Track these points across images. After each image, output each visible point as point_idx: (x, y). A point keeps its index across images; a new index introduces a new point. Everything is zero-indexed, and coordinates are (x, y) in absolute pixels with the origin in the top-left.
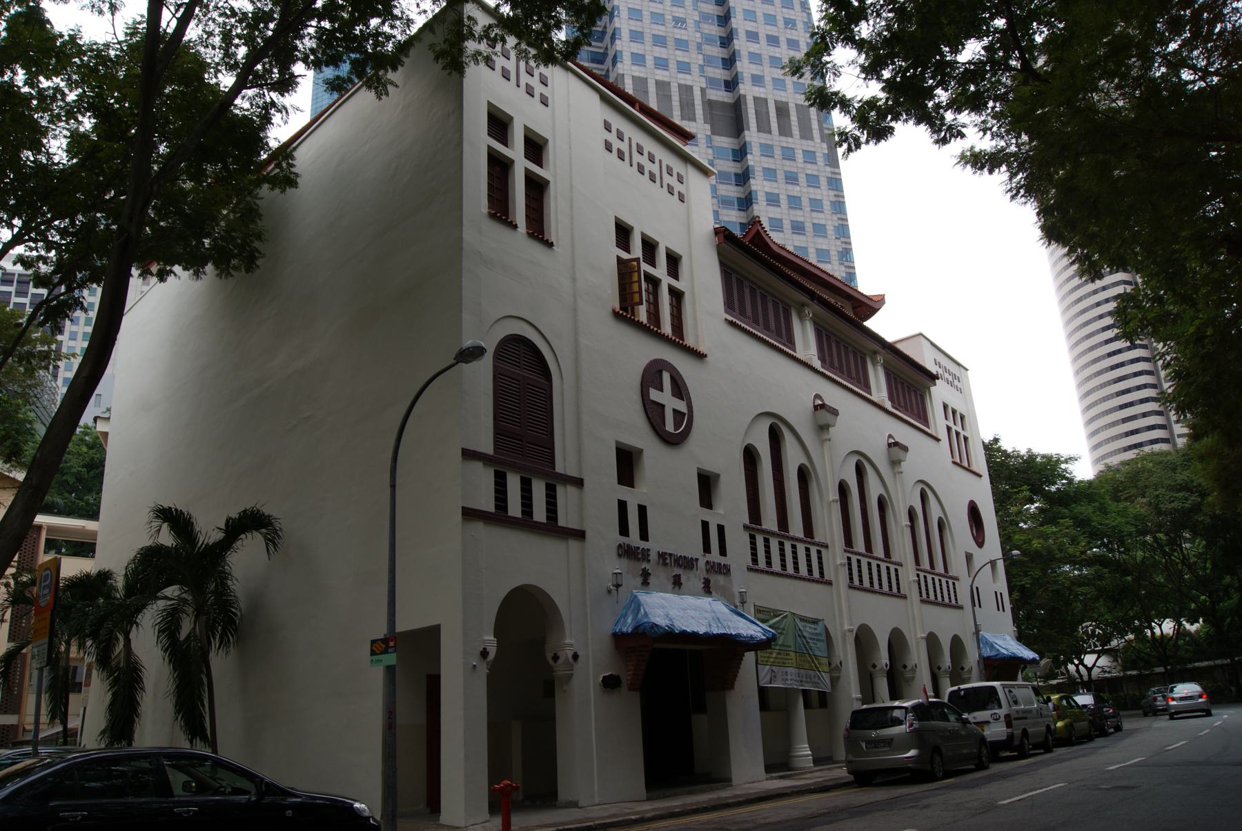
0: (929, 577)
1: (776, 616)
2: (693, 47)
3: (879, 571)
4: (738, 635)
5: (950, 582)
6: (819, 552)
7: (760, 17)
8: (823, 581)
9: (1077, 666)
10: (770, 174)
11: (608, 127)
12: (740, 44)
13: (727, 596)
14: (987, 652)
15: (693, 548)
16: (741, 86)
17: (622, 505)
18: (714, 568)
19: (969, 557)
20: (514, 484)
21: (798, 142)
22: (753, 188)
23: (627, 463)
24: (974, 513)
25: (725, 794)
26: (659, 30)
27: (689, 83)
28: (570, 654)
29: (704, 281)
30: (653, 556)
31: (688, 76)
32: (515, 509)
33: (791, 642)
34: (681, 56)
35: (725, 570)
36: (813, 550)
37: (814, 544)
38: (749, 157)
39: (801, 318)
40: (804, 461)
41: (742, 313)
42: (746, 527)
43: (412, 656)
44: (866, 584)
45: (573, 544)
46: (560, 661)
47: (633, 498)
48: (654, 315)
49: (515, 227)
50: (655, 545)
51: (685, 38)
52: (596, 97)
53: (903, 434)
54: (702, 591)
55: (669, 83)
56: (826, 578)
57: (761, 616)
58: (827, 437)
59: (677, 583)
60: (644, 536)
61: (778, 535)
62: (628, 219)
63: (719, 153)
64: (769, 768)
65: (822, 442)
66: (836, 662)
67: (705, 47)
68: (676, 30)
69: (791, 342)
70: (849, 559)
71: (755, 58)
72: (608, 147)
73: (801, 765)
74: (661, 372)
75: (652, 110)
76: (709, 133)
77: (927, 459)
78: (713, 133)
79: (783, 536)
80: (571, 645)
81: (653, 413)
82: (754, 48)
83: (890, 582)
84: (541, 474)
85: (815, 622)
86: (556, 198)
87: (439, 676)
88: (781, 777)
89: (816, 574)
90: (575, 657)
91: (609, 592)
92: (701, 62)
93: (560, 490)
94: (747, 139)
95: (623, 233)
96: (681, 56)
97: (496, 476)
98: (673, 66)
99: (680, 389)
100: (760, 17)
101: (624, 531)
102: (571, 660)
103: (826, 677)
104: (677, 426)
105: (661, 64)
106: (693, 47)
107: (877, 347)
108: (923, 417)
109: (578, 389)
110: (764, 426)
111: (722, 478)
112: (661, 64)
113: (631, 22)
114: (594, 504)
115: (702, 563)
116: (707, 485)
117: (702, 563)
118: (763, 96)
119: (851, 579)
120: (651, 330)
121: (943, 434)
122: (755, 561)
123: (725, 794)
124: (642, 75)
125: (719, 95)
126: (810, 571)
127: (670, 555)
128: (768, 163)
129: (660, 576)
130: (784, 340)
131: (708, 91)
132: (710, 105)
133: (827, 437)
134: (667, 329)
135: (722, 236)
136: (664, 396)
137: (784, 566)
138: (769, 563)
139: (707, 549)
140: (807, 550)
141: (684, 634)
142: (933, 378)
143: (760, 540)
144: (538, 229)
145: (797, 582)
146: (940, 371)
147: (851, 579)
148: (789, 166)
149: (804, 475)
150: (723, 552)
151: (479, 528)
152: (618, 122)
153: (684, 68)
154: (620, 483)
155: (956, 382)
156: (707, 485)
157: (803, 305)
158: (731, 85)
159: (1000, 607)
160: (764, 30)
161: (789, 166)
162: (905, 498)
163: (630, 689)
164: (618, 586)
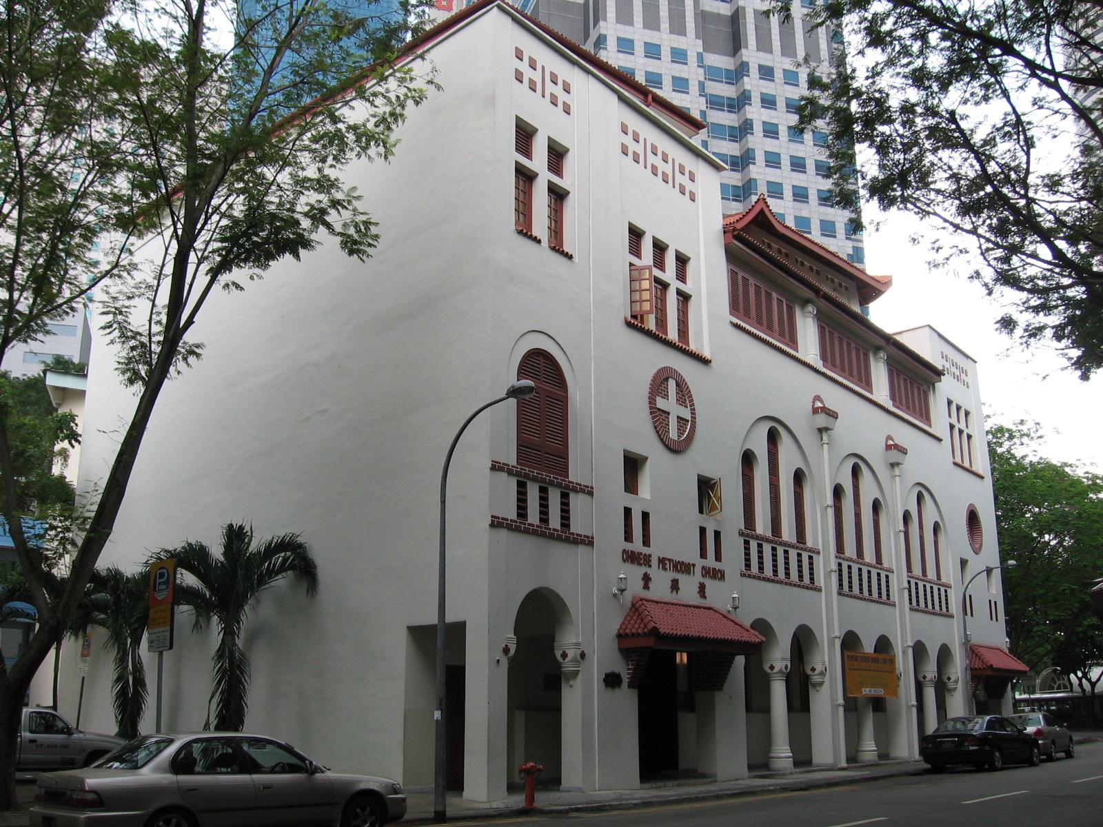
0: (921, 584)
3: (917, 589)
5: (943, 590)
6: (810, 558)
8: (813, 587)
9: (1080, 679)
11: (519, 55)
14: (978, 665)
15: (690, 554)
19: (964, 563)
24: (973, 519)
29: (710, 278)
32: (533, 517)
37: (806, 550)
43: (440, 648)
48: (662, 322)
50: (655, 551)
52: (614, 98)
53: (903, 435)
60: (646, 542)
61: (797, 548)
62: (640, 224)
64: (751, 767)
70: (840, 565)
72: (519, 77)
76: (701, 50)
77: (927, 460)
79: (775, 542)
81: (659, 417)
83: (880, 589)
87: (463, 668)
93: (572, 496)
99: (684, 395)
101: (628, 537)
104: (680, 434)
107: (881, 342)
108: (926, 416)
110: (764, 428)
114: (599, 514)
116: (706, 487)
119: (841, 585)
120: (658, 337)
121: (943, 432)
122: (748, 566)
123: (713, 788)
127: (670, 560)
130: (777, 334)
134: (673, 335)
136: (670, 403)
137: (775, 571)
138: (761, 569)
139: (703, 554)
142: (939, 373)
143: (753, 545)
145: (933, 617)
146: (947, 365)
147: (841, 585)
150: (718, 558)
151: (503, 533)
152: (533, 48)
154: (625, 491)
155: (963, 376)
159: (993, 615)
162: (899, 499)
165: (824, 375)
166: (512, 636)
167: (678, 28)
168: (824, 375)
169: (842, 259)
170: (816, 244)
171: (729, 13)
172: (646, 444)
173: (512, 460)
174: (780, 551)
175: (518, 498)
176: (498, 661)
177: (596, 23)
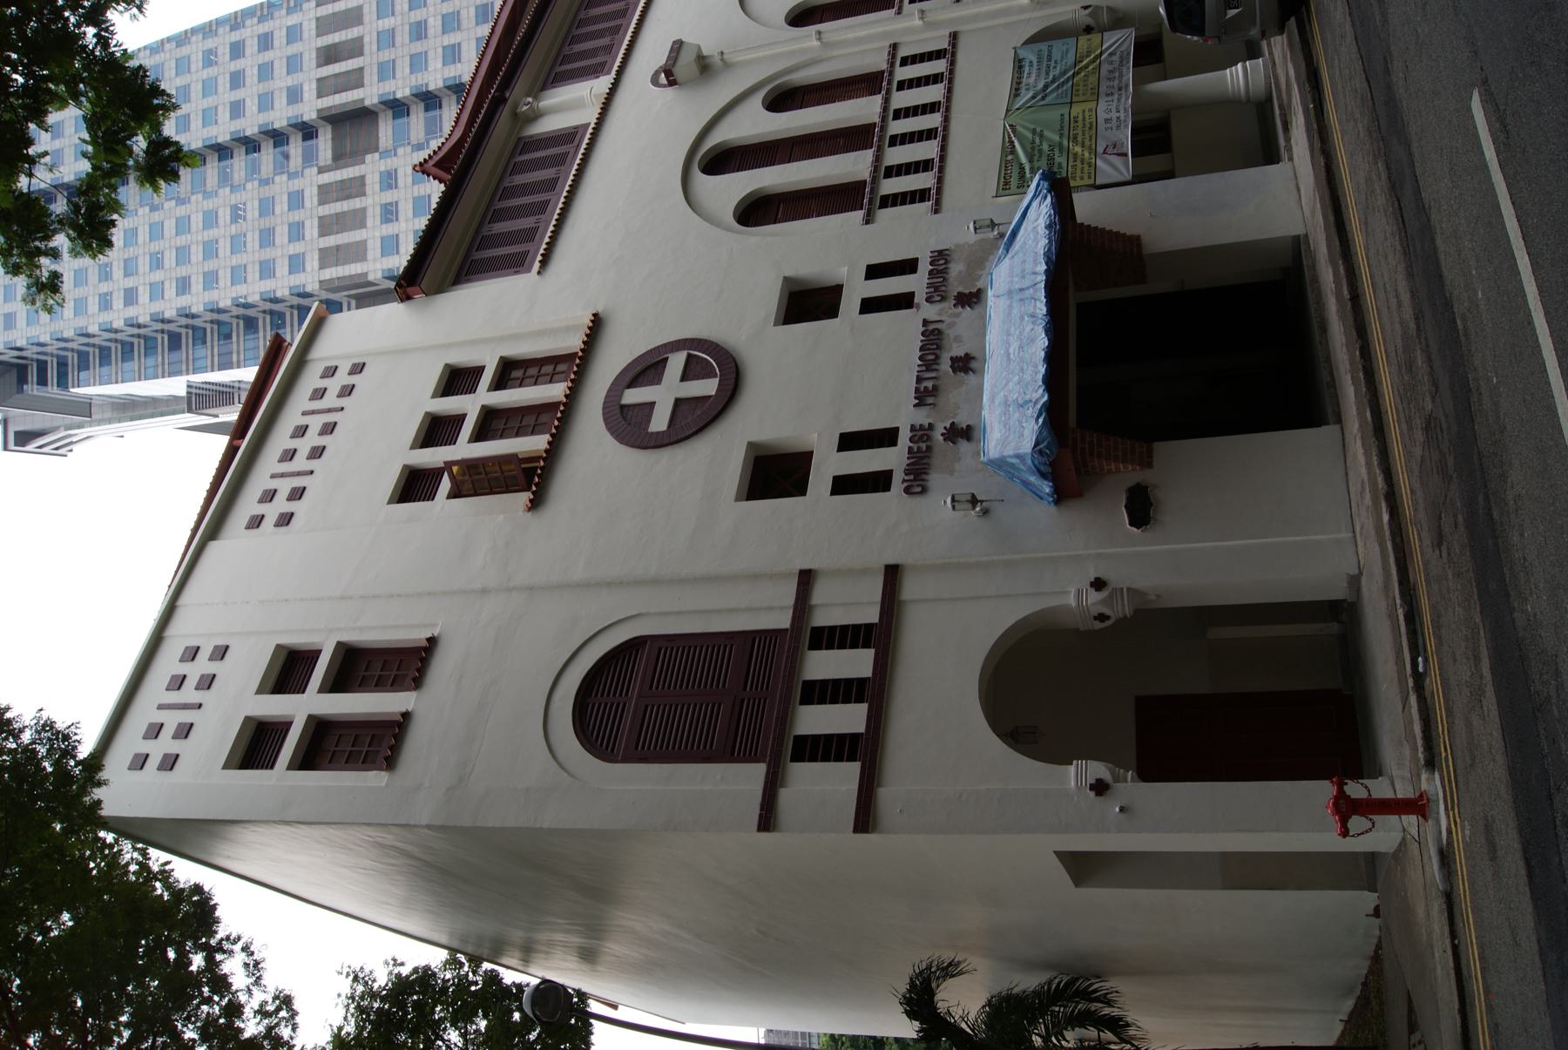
1: (1013, 151)
2: (267, 192)
4: (1047, 255)
6: (905, 62)
7: (209, 102)
10: (418, 62)
11: (256, 522)
12: (250, 126)
13: (981, 259)
16: (306, 119)
17: (844, 485)
18: (937, 292)
20: (816, 720)
21: (367, 27)
22: (440, 84)
23: (776, 474)
25: (1321, 246)
26: (253, 240)
27: (315, 191)
28: (1094, 597)
30: (922, 417)
31: (307, 194)
33: (1054, 115)
34: (281, 206)
35: (941, 258)
36: (904, 73)
38: (399, 95)
39: (536, 116)
40: (756, 102)
41: (530, 235)
42: (868, 220)
44: (933, 93)
45: (910, 589)
46: (1107, 611)
47: (858, 289)
49: (406, 715)
50: (904, 416)
51: (256, 203)
54: (978, 309)
55: (320, 218)
56: (944, 45)
57: (1014, 181)
58: (717, 59)
59: (965, 365)
60: (887, 437)
61: (888, 92)
62: (390, 479)
63: (401, 139)
64: (1269, 153)
65: (727, 65)
66: (1084, 18)
67: (264, 175)
68: (249, 216)
69: (569, 137)
71: (265, 102)
73: (1262, 81)
74: (624, 408)
75: (241, 416)
76: (377, 155)
78: (376, 149)
80: (1079, 593)
81: (693, 420)
82: (251, 106)
84: (795, 663)
85: (1019, 64)
86: (361, 629)
88: (1286, 128)
89: (939, 66)
90: (1098, 584)
91: (985, 512)
92: (285, 177)
93: (824, 617)
94: (375, 101)
95: (415, 486)
96: (281, 206)
97: (819, 648)
98: (297, 216)
99: (647, 369)
100: (209, 102)
102: (1104, 594)
103: (1112, 39)
105: (296, 232)
106: (267, 192)
109: (656, 582)
110: (706, 184)
111: (789, 273)
112: (296, 232)
113: (249, 279)
115: (930, 312)
116: (808, 302)
117: (930, 312)
118: (314, 86)
120: (557, 420)
123: (1321, 246)
124: (316, 257)
125: (324, 144)
126: (934, 79)
127: (919, 380)
128: (403, 68)
129: (955, 393)
131: (322, 164)
132: (341, 157)
133: (717, 59)
135: (409, 290)
136: (662, 396)
139: (903, 301)
140: (902, 86)
141: (1053, 381)
144: (405, 664)
148: (402, 37)
149: (783, 99)
150: (909, 266)
151: (889, 796)
153: (296, 200)
154: (836, 316)
156: (808, 302)
157: (515, 115)
158: (308, 131)
160: (226, 96)
161: (402, 37)
163: (1150, 465)
164: (974, 501)
165: (620, 72)
166: (1072, 769)
167: (355, 188)
168: (620, 72)
169: (493, 29)
170: (477, 68)
171: (329, 128)
172: (722, 454)
173: (859, 215)
174: (898, 127)
175: (823, 760)
176: (1122, 809)
177: (371, 284)
